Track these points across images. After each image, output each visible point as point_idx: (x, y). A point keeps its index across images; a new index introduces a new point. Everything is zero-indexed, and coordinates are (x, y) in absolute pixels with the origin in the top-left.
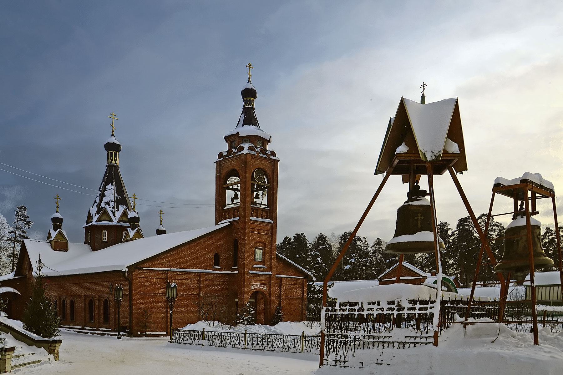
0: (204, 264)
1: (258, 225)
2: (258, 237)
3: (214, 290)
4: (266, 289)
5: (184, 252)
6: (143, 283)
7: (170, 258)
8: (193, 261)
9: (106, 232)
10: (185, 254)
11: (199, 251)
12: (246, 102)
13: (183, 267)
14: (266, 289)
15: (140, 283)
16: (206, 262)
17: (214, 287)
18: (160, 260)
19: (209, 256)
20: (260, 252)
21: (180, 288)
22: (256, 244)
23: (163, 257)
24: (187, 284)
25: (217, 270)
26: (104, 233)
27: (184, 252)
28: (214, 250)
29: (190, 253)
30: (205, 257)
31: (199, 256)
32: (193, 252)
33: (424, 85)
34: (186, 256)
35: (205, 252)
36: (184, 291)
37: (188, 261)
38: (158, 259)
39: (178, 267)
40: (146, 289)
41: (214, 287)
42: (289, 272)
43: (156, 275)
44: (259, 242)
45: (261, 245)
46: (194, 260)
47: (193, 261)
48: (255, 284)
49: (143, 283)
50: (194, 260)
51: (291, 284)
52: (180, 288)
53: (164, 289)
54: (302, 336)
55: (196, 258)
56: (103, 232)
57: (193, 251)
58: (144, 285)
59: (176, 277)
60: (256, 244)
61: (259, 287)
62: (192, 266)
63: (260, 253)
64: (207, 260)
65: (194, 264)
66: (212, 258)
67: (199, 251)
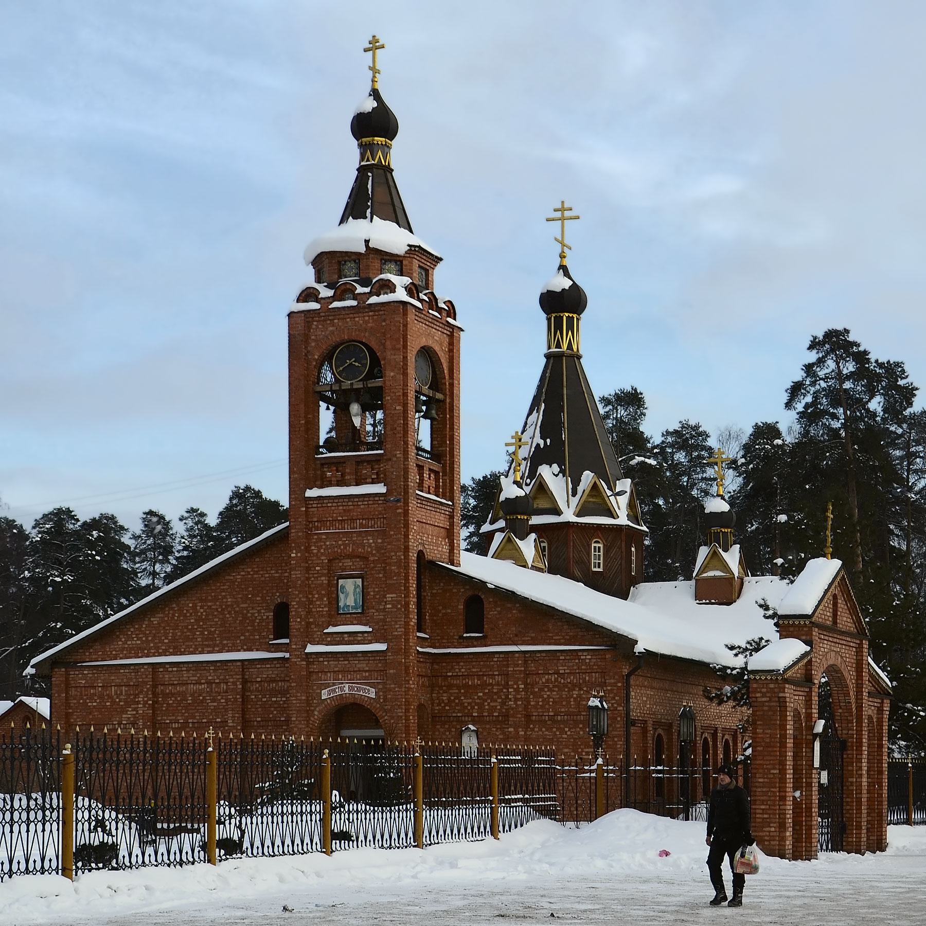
0: (242, 638)
1: (341, 508)
2: (340, 542)
3: (276, 706)
4: (373, 695)
5: (185, 611)
6: (81, 701)
7: (147, 632)
8: (210, 632)
9: (601, 546)
10: (188, 615)
11: (227, 602)
12: (365, 149)
13: (185, 651)
14: (373, 695)
15: (76, 701)
16: (248, 631)
17: (274, 699)
18: (123, 640)
19: (259, 612)
20: (356, 587)
21: (177, 707)
22: (340, 564)
23: (132, 630)
24: (196, 695)
25: (283, 649)
26: (595, 547)
27: (185, 611)
28: (274, 594)
29: (202, 610)
30: (245, 617)
31: (228, 616)
32: (210, 607)
33: (374, 46)
34: (192, 621)
35: (246, 603)
36: (187, 714)
37: (198, 633)
38: (118, 637)
39: (171, 650)
40: (90, 713)
41: (274, 699)
42: (547, 631)
43: (113, 678)
44: (351, 556)
45: (359, 563)
46: (213, 630)
47: (210, 632)
48: (334, 684)
49: (81, 701)
50: (213, 630)
51: (557, 673)
52: (177, 707)
53: (135, 712)
54: (325, 821)
55: (219, 623)
56: (593, 545)
57: (209, 604)
58: (85, 703)
59: (167, 679)
60: (340, 564)
61: (347, 691)
62: (208, 646)
63: (355, 588)
64: (253, 626)
65: (214, 639)
66: (268, 617)
67: (227, 602)
